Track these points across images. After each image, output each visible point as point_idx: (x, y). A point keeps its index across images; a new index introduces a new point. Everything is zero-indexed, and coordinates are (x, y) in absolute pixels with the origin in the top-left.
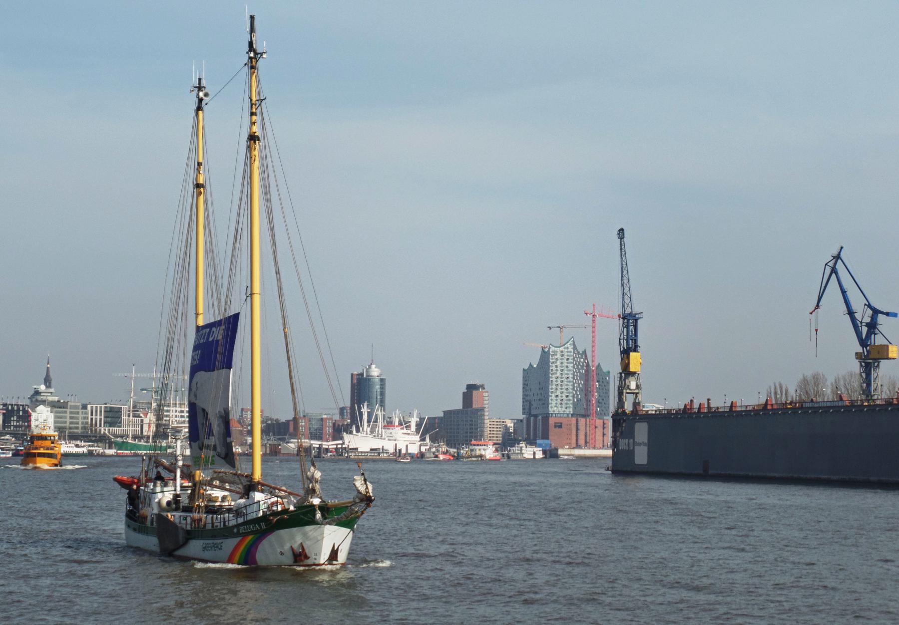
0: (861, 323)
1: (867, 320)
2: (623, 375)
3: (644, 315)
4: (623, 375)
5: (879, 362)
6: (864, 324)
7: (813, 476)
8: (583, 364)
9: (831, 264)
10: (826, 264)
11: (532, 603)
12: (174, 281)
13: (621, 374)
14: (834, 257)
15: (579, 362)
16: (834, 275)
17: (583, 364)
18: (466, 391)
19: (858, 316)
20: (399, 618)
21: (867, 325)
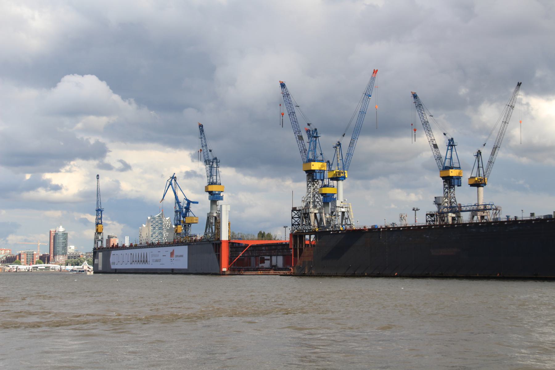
0: (183, 207)
1: (185, 205)
2: (97, 233)
3: (104, 210)
4: (97, 233)
5: (191, 225)
6: (184, 207)
7: (482, 276)
8: (168, 224)
9: (170, 181)
10: (168, 180)
11: (94, 316)
12: (500, 120)
13: (96, 233)
14: (171, 177)
15: (166, 224)
16: (170, 185)
17: (168, 224)
18: (107, 238)
19: (181, 204)
20: (131, 325)
21: (185, 208)
